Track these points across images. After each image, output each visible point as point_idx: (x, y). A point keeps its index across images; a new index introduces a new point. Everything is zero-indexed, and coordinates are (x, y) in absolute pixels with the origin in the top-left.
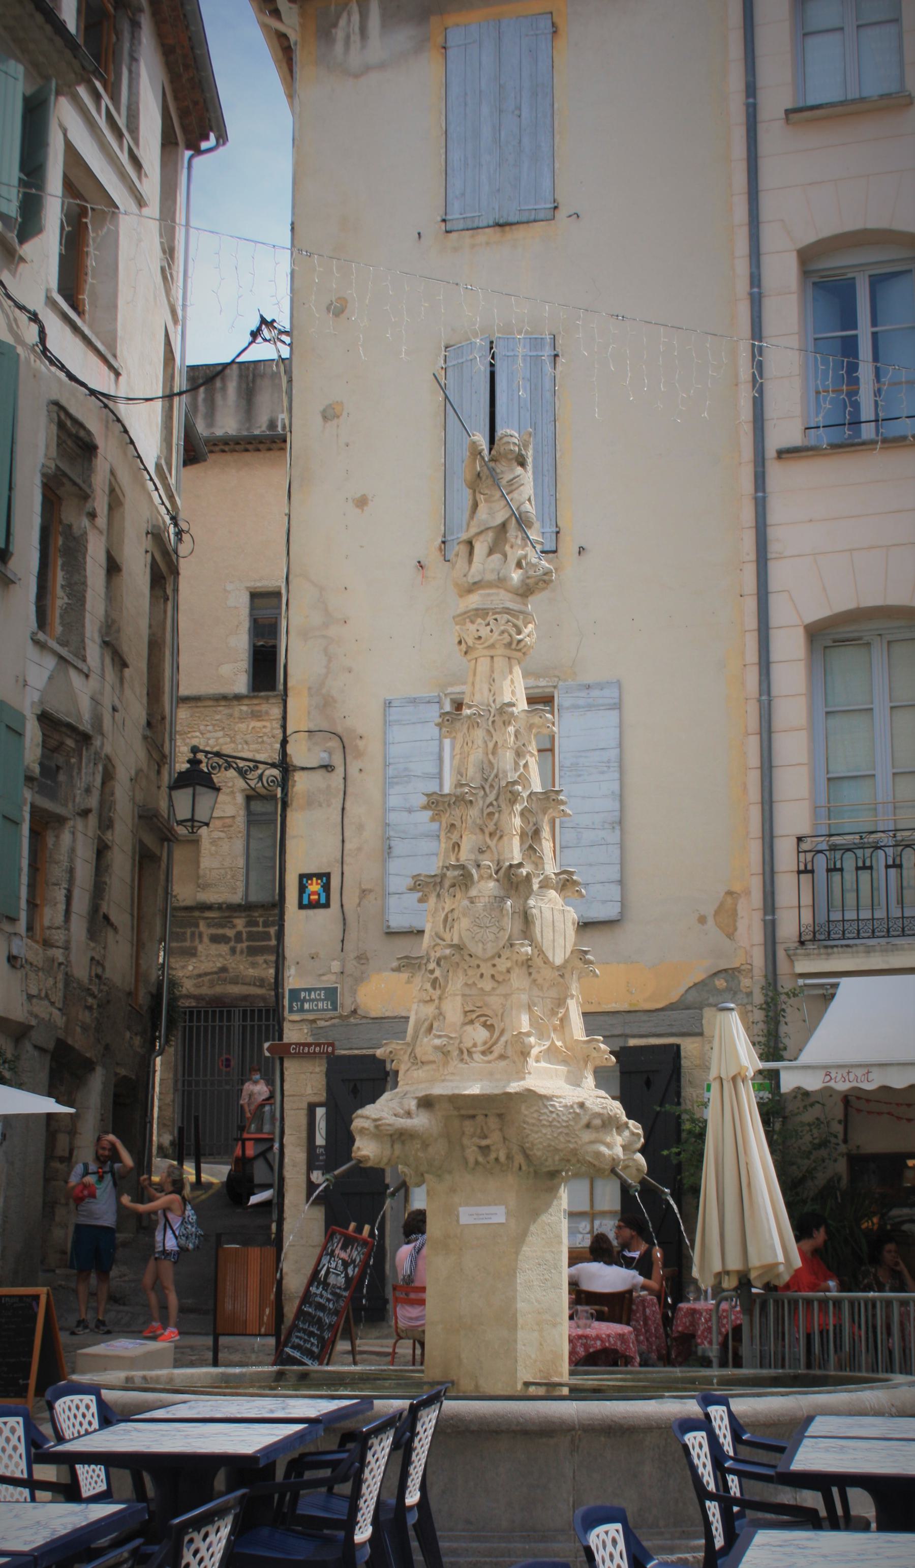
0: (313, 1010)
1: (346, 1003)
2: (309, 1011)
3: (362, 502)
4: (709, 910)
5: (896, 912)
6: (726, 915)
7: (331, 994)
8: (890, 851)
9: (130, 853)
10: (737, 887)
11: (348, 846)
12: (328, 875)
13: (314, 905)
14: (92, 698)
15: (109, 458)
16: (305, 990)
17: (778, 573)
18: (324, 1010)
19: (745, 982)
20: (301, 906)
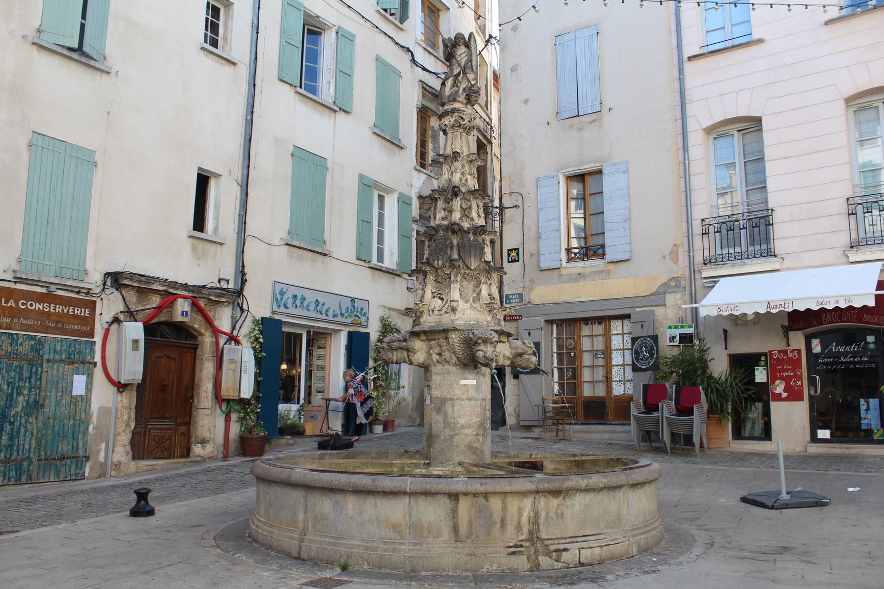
1: (526, 299)
3: (526, 102)
4: (667, 253)
5: (719, 252)
6: (674, 255)
7: (521, 296)
8: (716, 226)
10: (678, 243)
13: (514, 261)
17: (690, 109)
19: (683, 282)
20: (509, 262)
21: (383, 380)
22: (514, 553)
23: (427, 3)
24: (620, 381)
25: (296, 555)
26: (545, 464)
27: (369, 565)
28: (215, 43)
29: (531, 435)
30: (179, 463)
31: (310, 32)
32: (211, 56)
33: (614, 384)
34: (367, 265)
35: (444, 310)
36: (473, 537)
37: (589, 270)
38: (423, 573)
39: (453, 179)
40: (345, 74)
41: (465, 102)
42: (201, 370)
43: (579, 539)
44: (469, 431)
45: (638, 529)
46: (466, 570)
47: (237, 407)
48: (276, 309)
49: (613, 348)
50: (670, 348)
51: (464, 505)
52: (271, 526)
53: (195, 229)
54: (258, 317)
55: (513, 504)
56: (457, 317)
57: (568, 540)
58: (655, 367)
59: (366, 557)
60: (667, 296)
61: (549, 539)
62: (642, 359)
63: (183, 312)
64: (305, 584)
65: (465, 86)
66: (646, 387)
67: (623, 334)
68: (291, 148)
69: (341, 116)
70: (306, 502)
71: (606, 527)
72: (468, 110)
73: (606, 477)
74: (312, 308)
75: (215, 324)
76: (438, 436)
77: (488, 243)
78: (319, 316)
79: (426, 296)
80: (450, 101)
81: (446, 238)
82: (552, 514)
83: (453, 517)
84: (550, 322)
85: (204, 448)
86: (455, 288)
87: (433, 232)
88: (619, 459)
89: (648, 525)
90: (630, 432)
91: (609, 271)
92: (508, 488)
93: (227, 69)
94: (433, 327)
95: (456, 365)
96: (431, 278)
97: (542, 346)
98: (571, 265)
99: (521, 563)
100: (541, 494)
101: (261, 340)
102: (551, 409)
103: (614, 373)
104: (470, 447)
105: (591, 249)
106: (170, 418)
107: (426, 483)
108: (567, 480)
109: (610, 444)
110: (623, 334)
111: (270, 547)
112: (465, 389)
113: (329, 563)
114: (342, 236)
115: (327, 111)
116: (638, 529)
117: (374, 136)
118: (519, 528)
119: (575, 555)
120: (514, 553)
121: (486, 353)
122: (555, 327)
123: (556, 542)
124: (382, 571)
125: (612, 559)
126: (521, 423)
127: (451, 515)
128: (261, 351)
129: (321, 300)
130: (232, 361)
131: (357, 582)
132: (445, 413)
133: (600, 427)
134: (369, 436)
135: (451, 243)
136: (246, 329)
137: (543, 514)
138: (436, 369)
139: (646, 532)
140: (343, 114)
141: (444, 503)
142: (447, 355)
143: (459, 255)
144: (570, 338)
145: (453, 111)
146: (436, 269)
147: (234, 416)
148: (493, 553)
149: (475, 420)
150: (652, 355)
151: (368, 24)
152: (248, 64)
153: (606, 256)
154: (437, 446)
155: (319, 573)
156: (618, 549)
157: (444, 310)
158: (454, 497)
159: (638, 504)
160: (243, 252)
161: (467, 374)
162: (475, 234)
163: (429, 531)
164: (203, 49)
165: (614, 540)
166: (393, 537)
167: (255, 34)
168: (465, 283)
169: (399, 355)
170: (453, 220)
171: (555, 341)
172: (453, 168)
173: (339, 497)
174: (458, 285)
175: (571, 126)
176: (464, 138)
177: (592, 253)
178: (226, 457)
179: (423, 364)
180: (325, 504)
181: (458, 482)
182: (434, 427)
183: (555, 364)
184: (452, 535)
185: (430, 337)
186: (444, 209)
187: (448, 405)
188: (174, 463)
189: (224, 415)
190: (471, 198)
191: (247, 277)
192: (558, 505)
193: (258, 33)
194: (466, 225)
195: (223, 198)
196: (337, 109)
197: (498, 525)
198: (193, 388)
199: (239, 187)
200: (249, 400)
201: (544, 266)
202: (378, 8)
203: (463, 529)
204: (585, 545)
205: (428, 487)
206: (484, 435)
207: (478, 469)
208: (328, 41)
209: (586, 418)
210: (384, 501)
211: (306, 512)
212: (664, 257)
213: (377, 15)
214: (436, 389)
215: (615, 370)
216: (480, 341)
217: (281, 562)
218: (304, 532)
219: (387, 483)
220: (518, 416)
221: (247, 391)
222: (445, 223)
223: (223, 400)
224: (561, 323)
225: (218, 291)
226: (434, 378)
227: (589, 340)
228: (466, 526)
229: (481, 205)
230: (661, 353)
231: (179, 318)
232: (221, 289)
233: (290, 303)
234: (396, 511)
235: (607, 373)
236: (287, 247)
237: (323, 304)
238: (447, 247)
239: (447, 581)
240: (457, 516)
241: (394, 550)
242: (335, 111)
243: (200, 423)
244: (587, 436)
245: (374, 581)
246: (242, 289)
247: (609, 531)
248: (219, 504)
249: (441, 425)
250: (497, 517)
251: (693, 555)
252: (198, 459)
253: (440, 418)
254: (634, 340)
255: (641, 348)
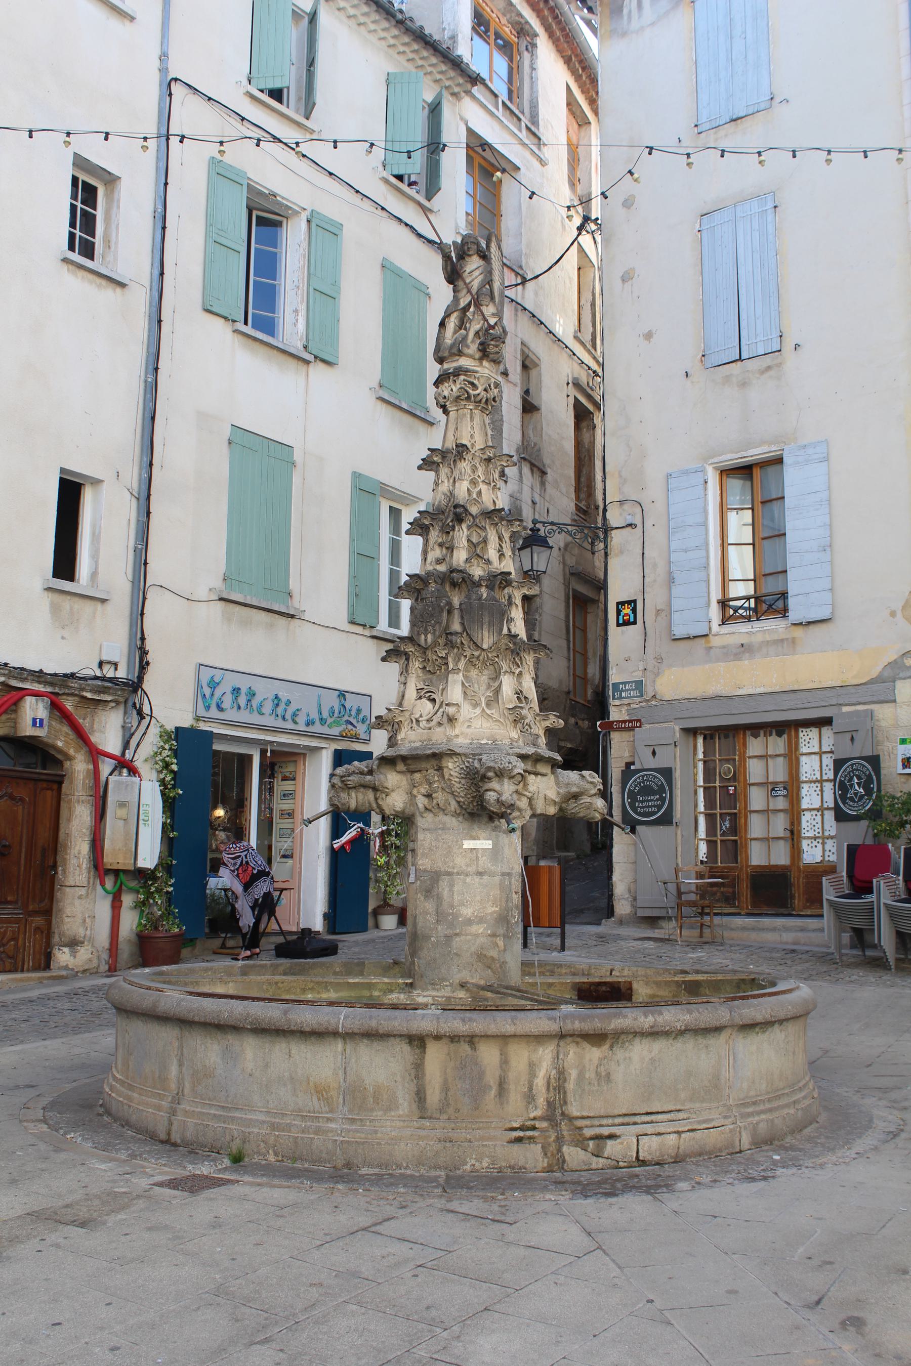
0: (628, 697)
1: (649, 692)
2: (624, 698)
3: (649, 336)
4: (898, 606)
7: (639, 685)
9: (563, 598)
11: (646, 580)
12: (635, 601)
13: (627, 623)
14: (511, 496)
15: (520, 335)
16: (622, 683)
18: (634, 697)
20: (618, 625)
21: (397, 835)
22: (519, 1140)
23: (477, 160)
24: (815, 838)
25: (163, 1136)
26: (635, 986)
27: (276, 1154)
28: (88, 251)
29: (657, 933)
30: (29, 979)
31: (262, 222)
32: (81, 273)
33: (805, 844)
34: (367, 633)
35: (436, 719)
36: (451, 1110)
37: (759, 638)
38: (364, 1171)
39: (456, 492)
40: (324, 295)
41: (478, 355)
42: (69, 820)
43: (638, 1119)
44: (479, 929)
45: (754, 1103)
46: (437, 1167)
47: (133, 884)
48: (202, 712)
49: (803, 778)
50: (903, 779)
51: (435, 1054)
52: (131, 1087)
53: (56, 574)
54: (170, 727)
55: (520, 1056)
56: (457, 731)
57: (618, 1120)
58: (875, 815)
59: (272, 1140)
60: (899, 684)
61: (583, 1118)
62: (852, 799)
63: (34, 720)
64: (160, 1184)
65: (478, 327)
66: (853, 851)
67: (821, 754)
68: (227, 432)
69: (317, 370)
70: (181, 1047)
71: (691, 1100)
72: (486, 370)
73: (690, 1012)
74: (268, 708)
75: (94, 739)
76: (428, 938)
77: (518, 601)
78: (280, 723)
79: (406, 697)
80: (452, 355)
81: (440, 595)
82: (590, 1074)
83: (417, 1077)
84: (692, 732)
85: (74, 954)
86: (455, 681)
87: (419, 586)
88: (753, 980)
89: (778, 1097)
90: (819, 931)
91: (793, 641)
92: (509, 1029)
93: (110, 294)
94: (416, 748)
95: (456, 814)
96: (416, 664)
97: (677, 775)
98: (726, 629)
99: (532, 1157)
100: (569, 1039)
101: (175, 767)
102: (693, 888)
103: (804, 824)
104: (481, 957)
105: (770, 603)
106: (16, 902)
107: (371, 1018)
108: (616, 1016)
109: (793, 951)
110: (821, 754)
111: (127, 1123)
112: (474, 856)
113: (215, 1150)
114: (321, 578)
115: (293, 363)
116: (754, 1103)
117: (379, 403)
118: (530, 1097)
119: (629, 1148)
120: (519, 1140)
121: (500, 794)
122: (700, 741)
123: (597, 1122)
124: (298, 1165)
125: (700, 1155)
126: (641, 913)
127: (413, 1072)
128: (174, 787)
129: (284, 696)
130: (122, 804)
131: (246, 1183)
132: (439, 898)
133: (779, 922)
134: (372, 934)
135: (449, 604)
136: (149, 746)
137: (573, 1074)
138: (422, 822)
139: (770, 1110)
140: (321, 366)
141: (403, 1052)
142: (440, 797)
143: (462, 624)
144: (727, 761)
145: (457, 372)
146: (424, 650)
147: (128, 900)
148: (482, 1138)
149: (490, 909)
150: (869, 792)
151: (367, 204)
152: (147, 284)
153: (791, 614)
154: (425, 954)
155: (190, 1167)
156: (712, 1138)
157: (436, 719)
158: (418, 1041)
159: (758, 1062)
160: (142, 614)
161: (476, 830)
162: (490, 587)
163: (377, 1099)
164: (65, 260)
165: (705, 1121)
166: (317, 1107)
167: (159, 231)
168: (474, 673)
169: (360, 796)
170: (455, 563)
171: (700, 765)
172: (456, 473)
173: (232, 1039)
174: (460, 677)
175: (727, 379)
176: (477, 420)
177: (765, 607)
178: (112, 969)
179: (403, 812)
180: (209, 1051)
181: (424, 1016)
182: (420, 924)
183: (701, 808)
184: (414, 1106)
185: (412, 767)
186: (441, 545)
187: (444, 883)
188: (21, 980)
189: (110, 898)
190: (487, 524)
191: (150, 657)
192: (601, 1059)
193: (164, 228)
194: (477, 572)
195: (105, 521)
196: (310, 357)
197: (493, 1092)
198: (55, 851)
199: (134, 501)
200: (153, 872)
201: (679, 632)
202: (385, 174)
203: (434, 1096)
204: (649, 1129)
205: (374, 1024)
206: (506, 936)
207: (489, 997)
208: (294, 238)
209: (755, 904)
210: (303, 1047)
211: (181, 1065)
212: (893, 614)
213: (383, 187)
214: (425, 855)
215: (806, 818)
216: (490, 774)
217: (134, 1147)
218: (177, 1099)
219: (306, 1017)
220: (635, 899)
221: (149, 855)
222: (442, 568)
223: (108, 871)
224: (711, 734)
225: (99, 683)
226: (420, 836)
227: (761, 762)
228: (437, 1092)
229: (507, 536)
230: (887, 789)
231: (27, 730)
232: (103, 679)
233: (227, 702)
234: (322, 1063)
235: (792, 824)
236: (222, 603)
237: (288, 703)
238: (441, 611)
239: (396, 1185)
240: (424, 1074)
241: (318, 1131)
242: (308, 362)
243: (68, 911)
244: (753, 935)
245: (276, 1182)
246: (141, 678)
247: (697, 1105)
248: (76, 1051)
249: (432, 918)
250: (491, 1078)
251: (852, 1153)
252: (64, 973)
253: (430, 906)
254: (838, 764)
255: (851, 779)
